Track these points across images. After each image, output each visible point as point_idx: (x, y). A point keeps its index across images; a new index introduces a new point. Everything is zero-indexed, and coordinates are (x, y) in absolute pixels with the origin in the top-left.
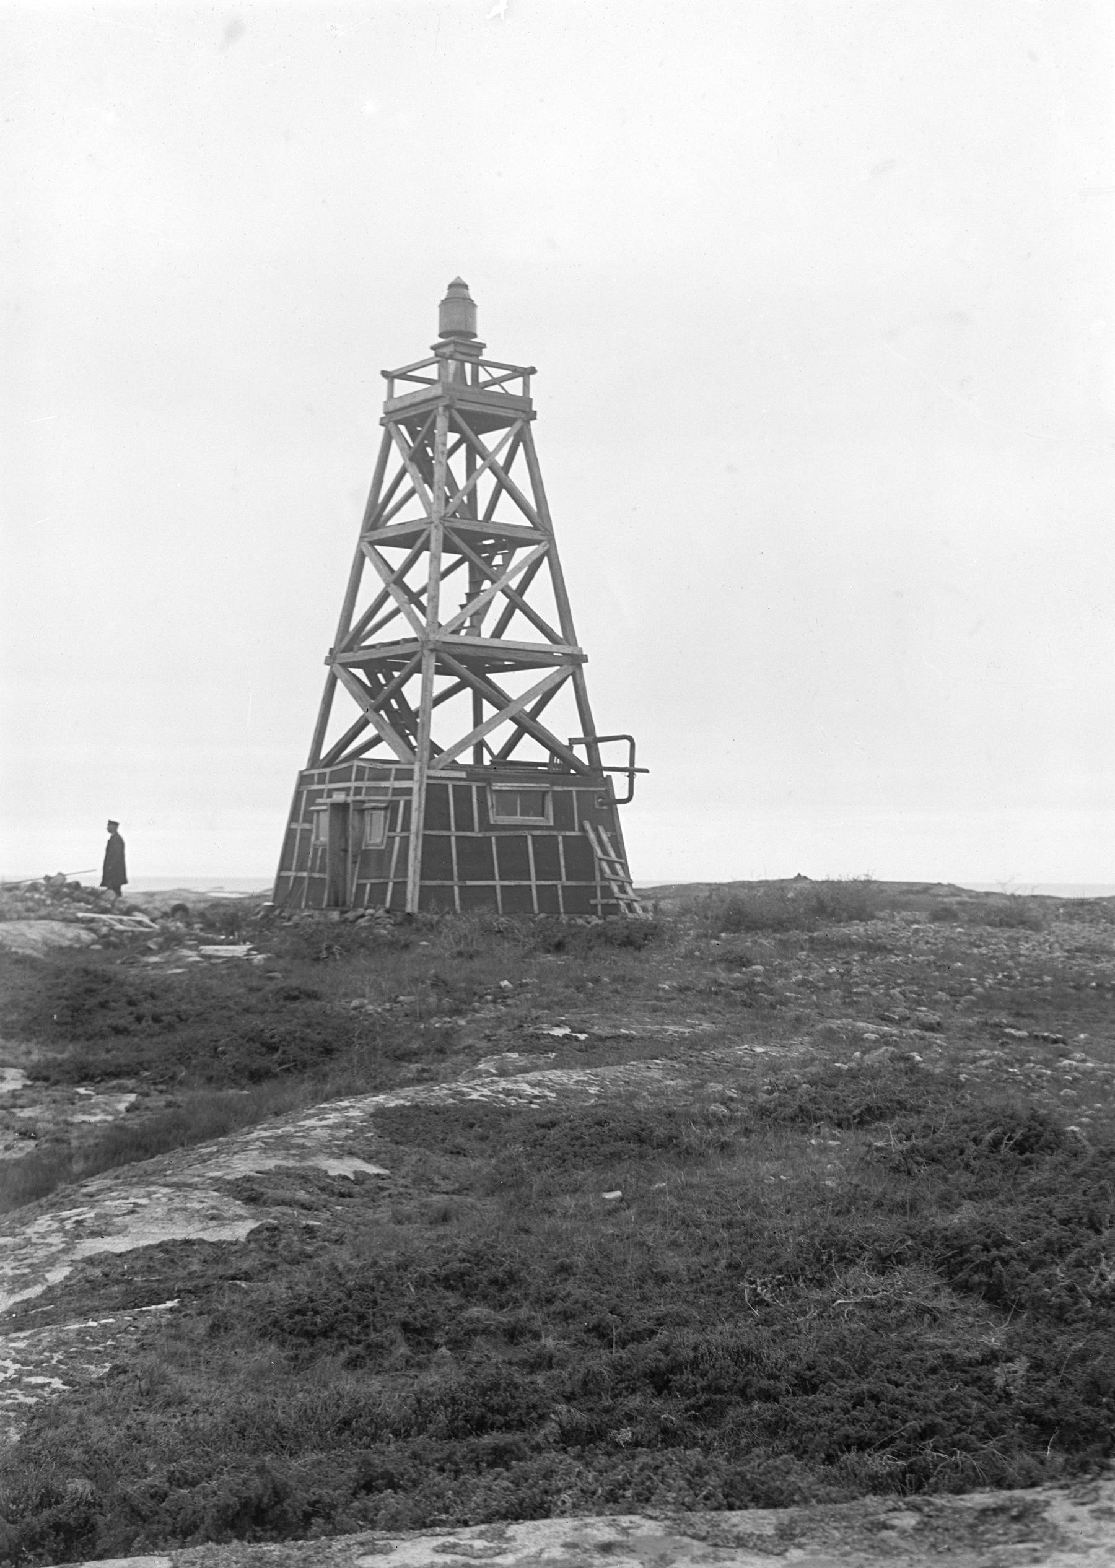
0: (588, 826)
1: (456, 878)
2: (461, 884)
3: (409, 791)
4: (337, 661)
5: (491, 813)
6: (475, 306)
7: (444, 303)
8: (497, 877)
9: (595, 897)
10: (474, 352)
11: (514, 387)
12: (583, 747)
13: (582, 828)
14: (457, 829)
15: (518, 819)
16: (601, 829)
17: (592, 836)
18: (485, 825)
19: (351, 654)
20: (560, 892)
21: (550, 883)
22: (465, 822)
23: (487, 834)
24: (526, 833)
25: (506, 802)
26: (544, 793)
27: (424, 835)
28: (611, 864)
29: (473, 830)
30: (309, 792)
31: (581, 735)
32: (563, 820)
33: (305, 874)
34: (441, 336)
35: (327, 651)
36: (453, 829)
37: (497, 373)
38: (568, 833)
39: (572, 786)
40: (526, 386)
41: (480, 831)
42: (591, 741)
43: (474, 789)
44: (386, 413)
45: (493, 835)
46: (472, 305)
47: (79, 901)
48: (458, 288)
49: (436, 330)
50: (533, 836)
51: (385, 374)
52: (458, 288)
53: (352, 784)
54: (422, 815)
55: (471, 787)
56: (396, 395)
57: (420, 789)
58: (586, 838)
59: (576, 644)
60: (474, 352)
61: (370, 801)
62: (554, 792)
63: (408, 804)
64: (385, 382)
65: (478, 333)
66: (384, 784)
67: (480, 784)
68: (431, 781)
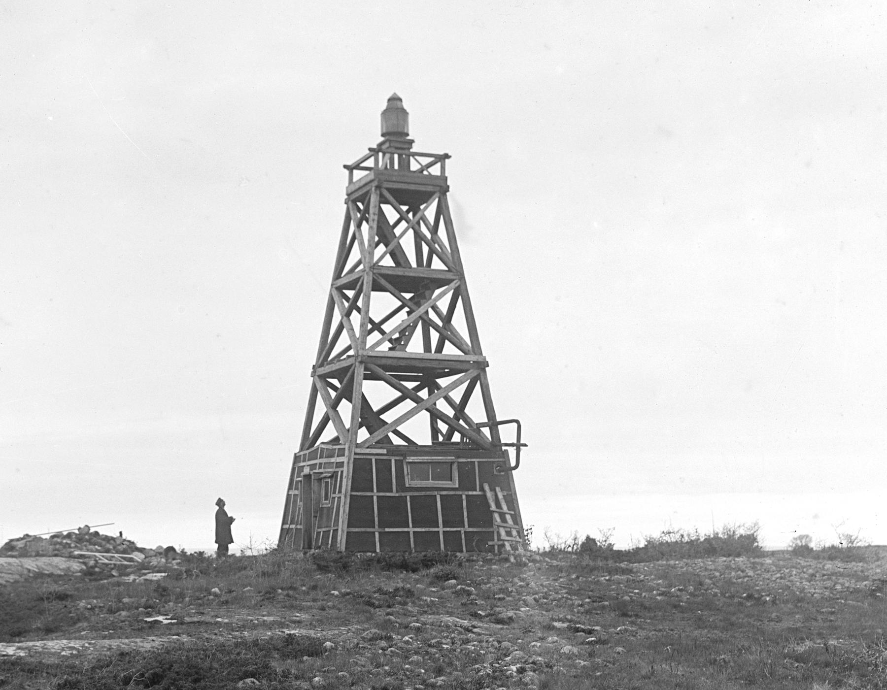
0: (486, 487)
1: (376, 527)
2: (380, 530)
3: (341, 465)
4: (317, 374)
5: (406, 478)
6: (408, 113)
7: (385, 113)
8: (411, 525)
9: (493, 540)
10: (406, 146)
11: (435, 170)
12: (488, 428)
13: (482, 489)
14: (378, 491)
15: (430, 483)
16: (498, 489)
17: (489, 494)
18: (401, 486)
19: (323, 368)
20: (463, 536)
21: (455, 529)
22: (384, 485)
23: (403, 494)
24: (436, 493)
25: (419, 470)
26: (452, 463)
27: (351, 496)
28: (502, 516)
29: (392, 492)
30: (298, 467)
31: (486, 420)
32: (467, 482)
33: (293, 526)
34: (383, 135)
35: (312, 367)
36: (375, 490)
37: (425, 161)
38: (470, 493)
39: (474, 458)
40: (443, 168)
41: (397, 492)
42: (493, 424)
43: (393, 461)
44: (348, 195)
45: (408, 495)
46: (405, 113)
47: (95, 545)
48: (395, 101)
49: (380, 133)
50: (441, 495)
51: (345, 167)
52: (395, 101)
53: (317, 461)
54: (350, 482)
55: (390, 460)
56: (355, 180)
57: (348, 463)
58: (484, 496)
59: (481, 354)
60: (406, 146)
61: (326, 472)
62: (458, 462)
63: (342, 472)
64: (347, 172)
65: (410, 133)
66: (333, 460)
67: (397, 458)
68: (357, 457)
